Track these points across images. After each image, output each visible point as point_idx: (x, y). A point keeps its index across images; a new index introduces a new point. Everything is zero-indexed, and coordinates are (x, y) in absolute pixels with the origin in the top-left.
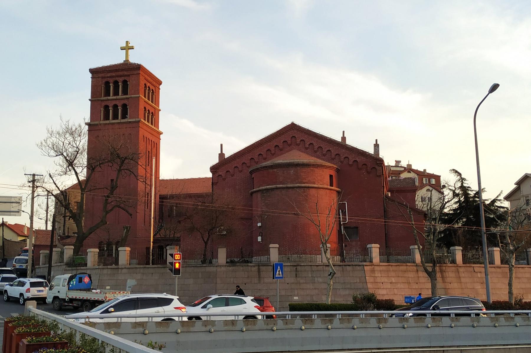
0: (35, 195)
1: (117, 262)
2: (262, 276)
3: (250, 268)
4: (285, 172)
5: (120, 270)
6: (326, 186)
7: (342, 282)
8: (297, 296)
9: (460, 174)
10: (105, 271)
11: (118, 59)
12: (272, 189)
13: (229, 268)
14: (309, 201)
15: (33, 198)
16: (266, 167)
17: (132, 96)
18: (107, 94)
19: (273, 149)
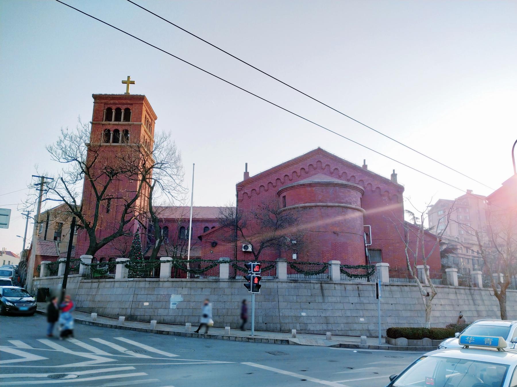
0: (43, 198)
1: (157, 274)
2: (326, 294)
3: (312, 285)
4: (324, 190)
5: (161, 283)
6: (358, 207)
7: (403, 303)
8: (363, 317)
9: (413, 214)
10: (142, 284)
11: (120, 90)
12: (311, 207)
13: (290, 284)
14: (300, 228)
15: (40, 202)
16: (304, 185)
17: (135, 123)
18: (109, 118)
19: (298, 171)
